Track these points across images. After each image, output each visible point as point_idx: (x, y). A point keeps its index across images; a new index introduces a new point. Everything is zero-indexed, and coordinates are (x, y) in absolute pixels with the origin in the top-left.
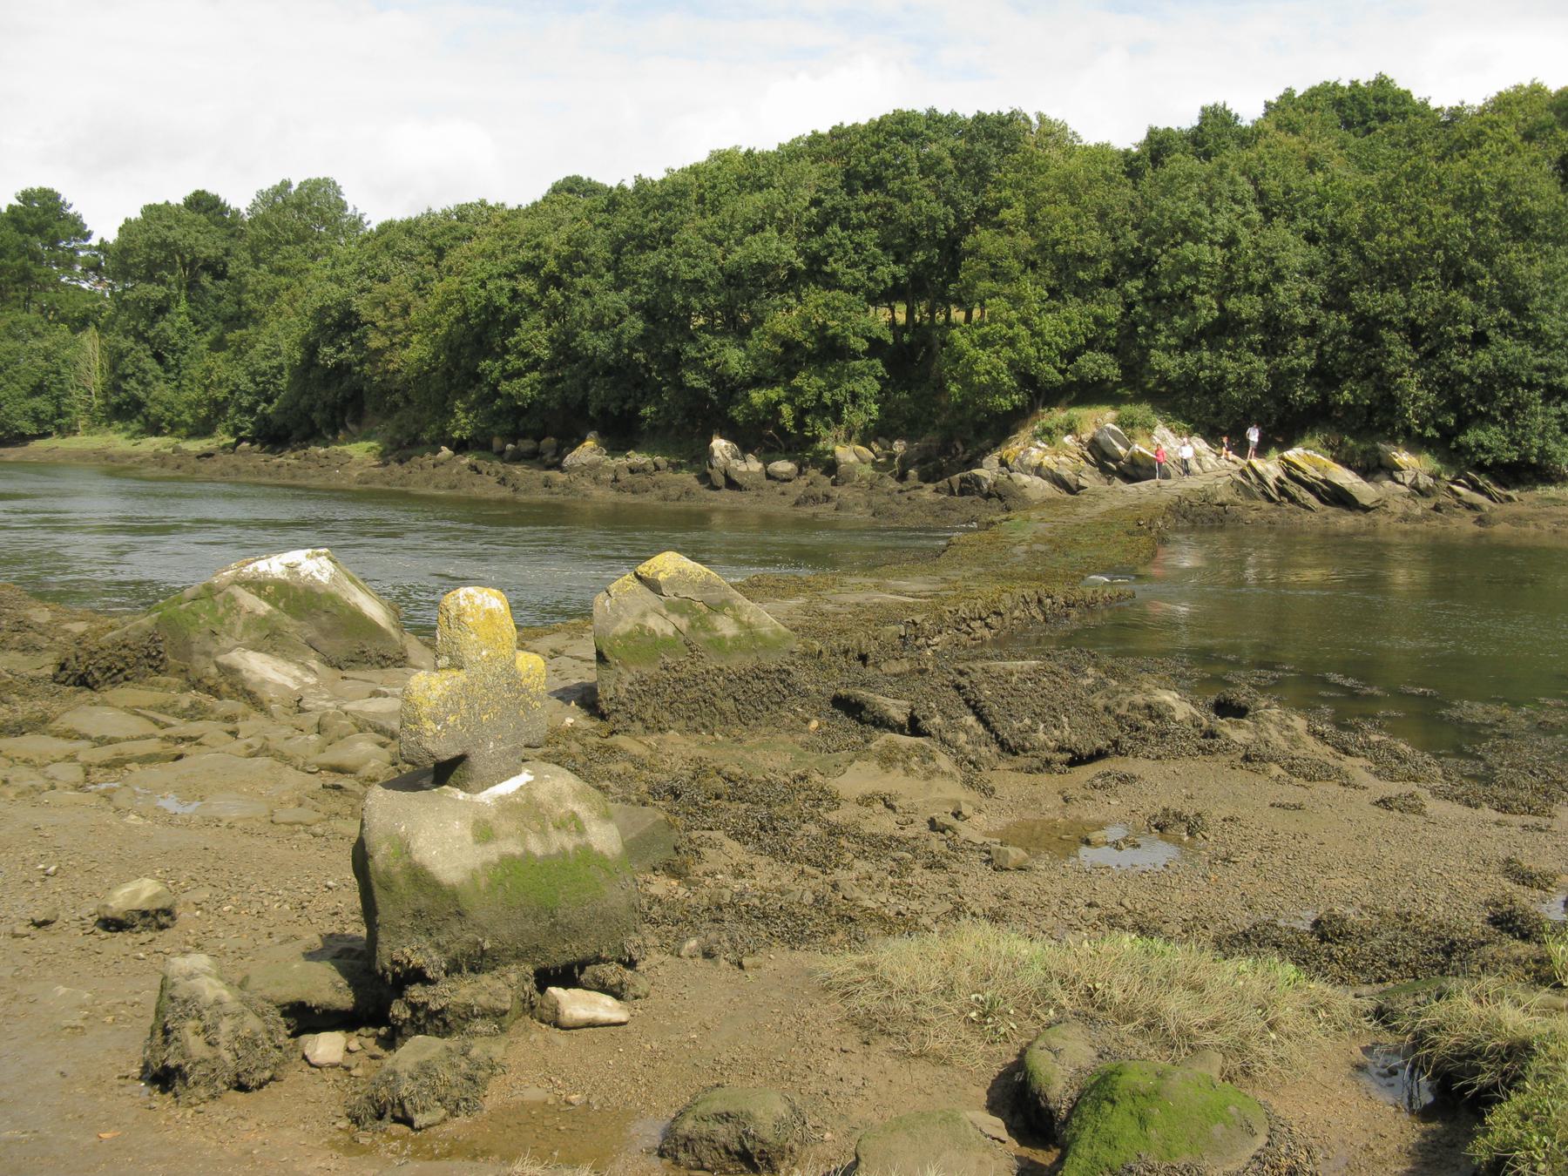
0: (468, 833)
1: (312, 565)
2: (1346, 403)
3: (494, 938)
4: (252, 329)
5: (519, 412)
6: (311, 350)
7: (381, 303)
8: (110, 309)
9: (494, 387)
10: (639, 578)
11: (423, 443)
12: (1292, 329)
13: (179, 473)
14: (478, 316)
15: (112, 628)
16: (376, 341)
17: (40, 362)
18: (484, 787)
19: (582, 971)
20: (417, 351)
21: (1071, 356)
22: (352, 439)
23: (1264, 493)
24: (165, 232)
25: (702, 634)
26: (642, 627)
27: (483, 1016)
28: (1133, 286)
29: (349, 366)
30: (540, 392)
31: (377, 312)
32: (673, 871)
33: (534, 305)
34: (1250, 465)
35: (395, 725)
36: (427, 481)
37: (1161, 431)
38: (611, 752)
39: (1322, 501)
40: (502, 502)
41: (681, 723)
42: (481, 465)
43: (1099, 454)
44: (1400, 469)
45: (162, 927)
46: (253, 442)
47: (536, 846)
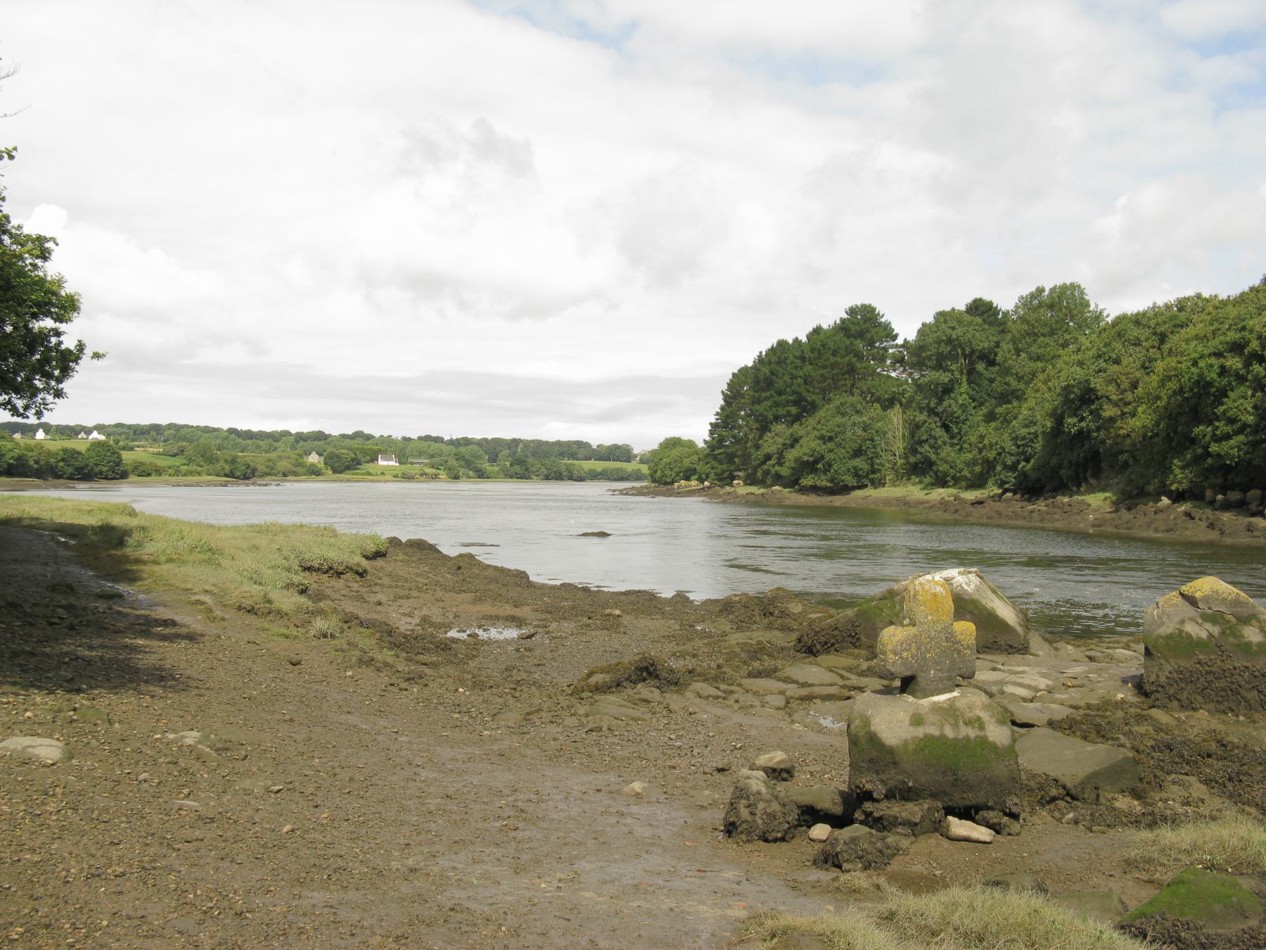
0: (907, 720)
1: (964, 579)
3: (915, 781)
4: (1015, 403)
5: (1227, 470)
6: (1059, 420)
7: (1113, 381)
8: (910, 391)
9: (1206, 447)
10: (1182, 595)
11: (1149, 494)
13: (956, 516)
14: (1191, 390)
15: (831, 617)
16: (1109, 411)
17: (860, 432)
18: (925, 697)
19: (977, 813)
20: (1141, 421)
22: (1092, 490)
24: (950, 331)
25: (1232, 640)
26: (1181, 631)
27: (904, 825)
29: (1089, 431)
30: (1246, 453)
31: (1110, 388)
32: (1136, 794)
33: (1241, 379)
35: (994, 689)
36: (1149, 525)
38: (1140, 719)
40: (1211, 544)
41: (1211, 706)
42: (1197, 513)
45: (785, 780)
46: (1015, 493)
47: (949, 732)
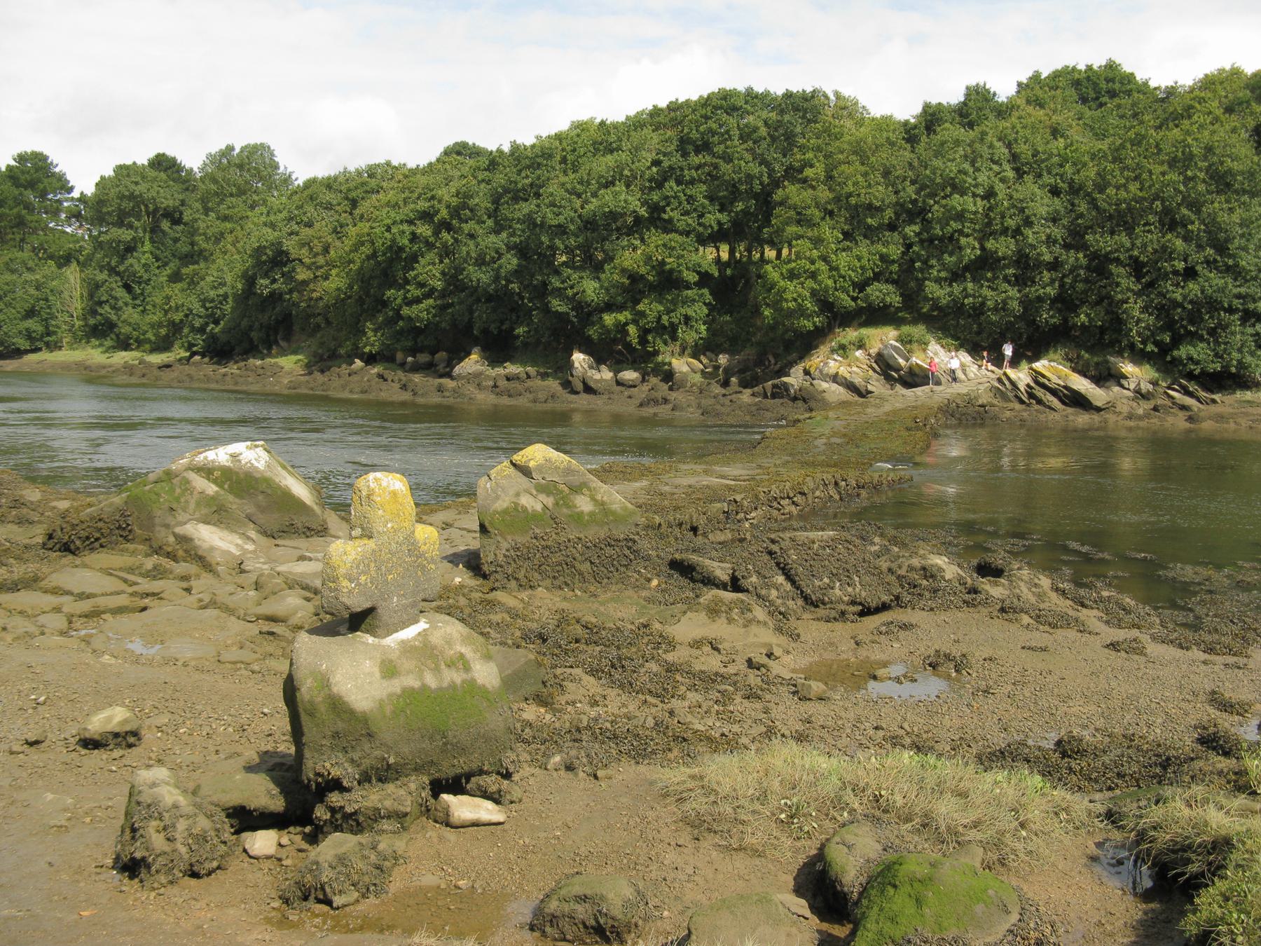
0: (376, 670)
1: (251, 455)
2: (1083, 324)
3: (397, 754)
4: (202, 265)
5: (418, 332)
6: (250, 281)
7: (306, 244)
8: (88, 249)
9: (397, 312)
10: (514, 465)
11: (340, 356)
12: (1039, 265)
13: (144, 380)
14: (384, 254)
15: (90, 505)
16: (302, 274)
17: (32, 291)
18: (389, 633)
19: (468, 781)
20: (335, 283)
21: (861, 286)
22: (283, 353)
23: (1016, 396)
24: (133, 187)
25: (565, 510)
26: (516, 504)
27: (389, 817)
28: (911, 230)
29: (281, 295)
30: (435, 316)
31: (303, 251)
32: (541, 700)
33: (430, 246)
34: (1005, 374)
35: (318, 583)
36: (344, 387)
37: (934, 347)
38: (491, 605)
39: (1063, 403)
40: (403, 404)
41: (548, 582)
42: (387, 374)
43: (884, 365)
44: (1126, 378)
45: (130, 746)
46: (203, 356)
47: (431, 681)
